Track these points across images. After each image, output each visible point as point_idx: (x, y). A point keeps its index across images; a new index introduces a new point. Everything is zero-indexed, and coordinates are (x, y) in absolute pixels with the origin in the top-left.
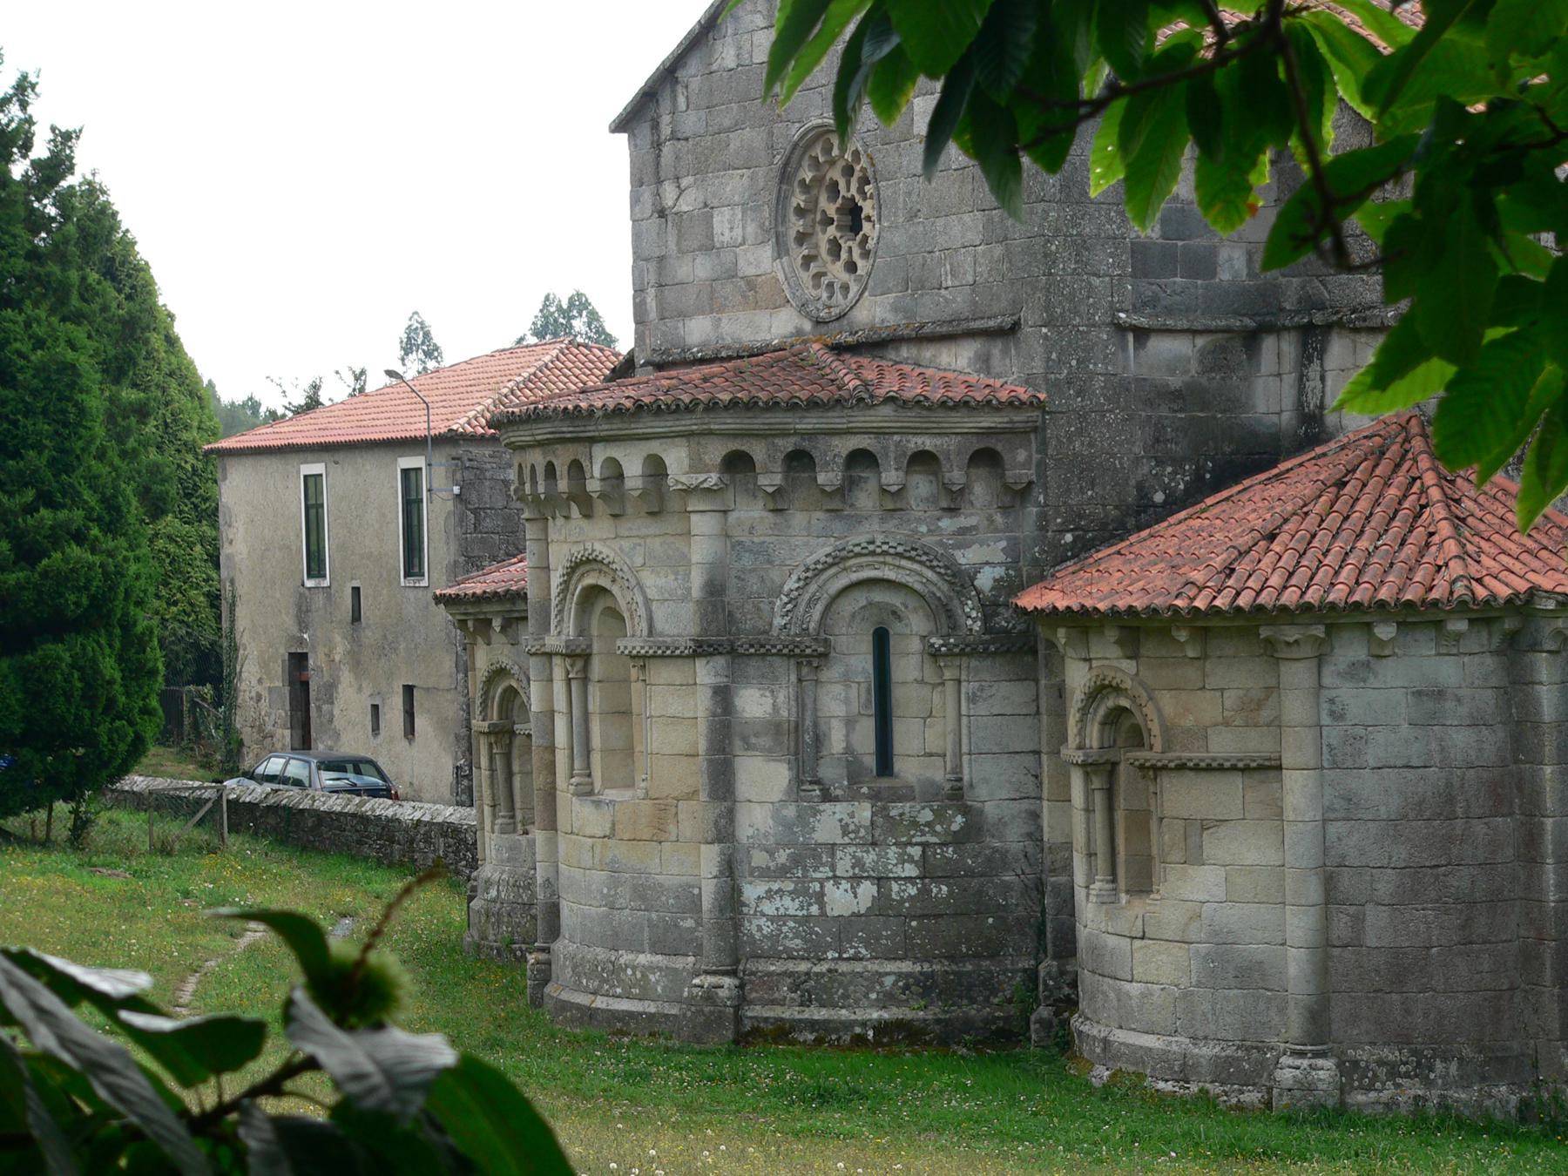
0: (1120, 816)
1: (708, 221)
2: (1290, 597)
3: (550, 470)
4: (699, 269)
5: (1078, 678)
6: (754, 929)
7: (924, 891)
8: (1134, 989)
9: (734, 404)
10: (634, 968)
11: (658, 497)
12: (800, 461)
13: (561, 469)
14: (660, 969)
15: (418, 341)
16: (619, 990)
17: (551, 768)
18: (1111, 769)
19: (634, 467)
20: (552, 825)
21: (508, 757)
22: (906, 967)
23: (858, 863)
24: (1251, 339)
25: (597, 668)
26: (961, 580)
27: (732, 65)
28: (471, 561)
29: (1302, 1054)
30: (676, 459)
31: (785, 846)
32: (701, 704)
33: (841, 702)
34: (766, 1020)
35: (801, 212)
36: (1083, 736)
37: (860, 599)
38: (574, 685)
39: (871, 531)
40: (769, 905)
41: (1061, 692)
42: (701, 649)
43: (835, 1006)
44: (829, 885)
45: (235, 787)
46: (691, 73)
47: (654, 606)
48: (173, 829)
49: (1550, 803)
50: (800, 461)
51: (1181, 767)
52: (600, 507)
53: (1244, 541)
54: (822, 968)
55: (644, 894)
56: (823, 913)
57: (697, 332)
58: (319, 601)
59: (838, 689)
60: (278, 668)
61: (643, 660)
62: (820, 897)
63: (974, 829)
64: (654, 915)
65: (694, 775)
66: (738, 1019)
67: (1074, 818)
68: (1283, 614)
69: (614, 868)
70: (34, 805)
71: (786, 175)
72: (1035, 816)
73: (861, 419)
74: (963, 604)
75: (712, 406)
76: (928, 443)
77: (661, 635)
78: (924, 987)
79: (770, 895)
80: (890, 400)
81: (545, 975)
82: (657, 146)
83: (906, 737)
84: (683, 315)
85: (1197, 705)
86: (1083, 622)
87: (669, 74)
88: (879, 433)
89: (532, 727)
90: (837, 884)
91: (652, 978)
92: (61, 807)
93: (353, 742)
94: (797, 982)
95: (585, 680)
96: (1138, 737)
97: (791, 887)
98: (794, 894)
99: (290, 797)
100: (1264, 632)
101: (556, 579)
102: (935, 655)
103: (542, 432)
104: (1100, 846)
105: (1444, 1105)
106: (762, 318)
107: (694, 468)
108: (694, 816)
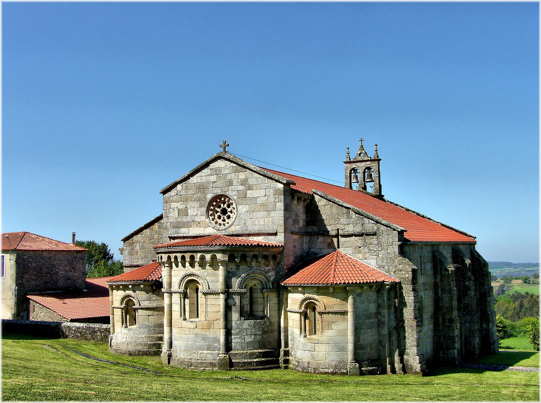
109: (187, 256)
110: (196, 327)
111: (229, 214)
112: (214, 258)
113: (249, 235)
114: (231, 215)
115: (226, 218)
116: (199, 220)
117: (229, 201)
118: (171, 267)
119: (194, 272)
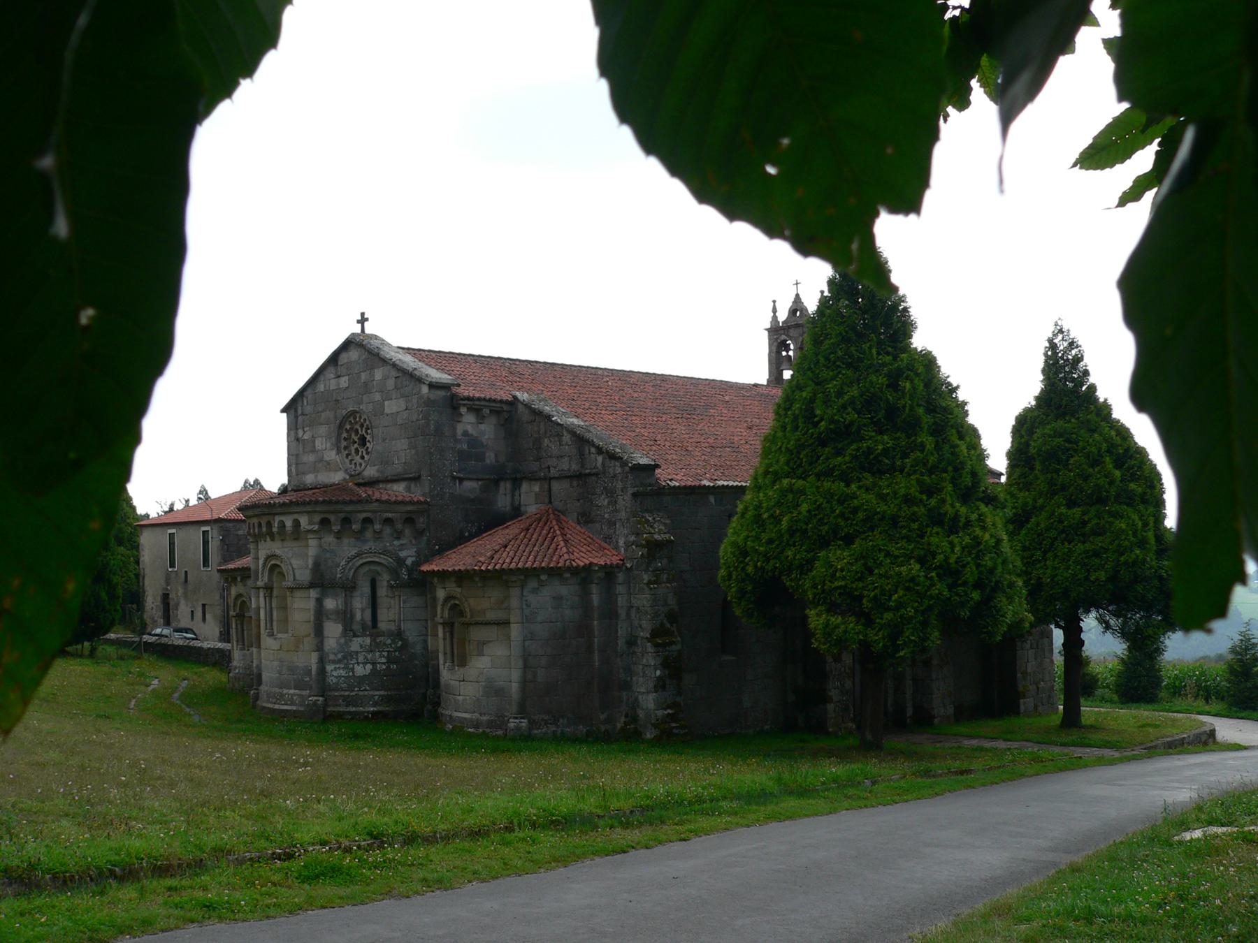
0: (455, 640)
1: (314, 442)
2: (513, 566)
3: (260, 525)
4: (311, 458)
5: (441, 594)
7: (388, 667)
8: (460, 698)
9: (324, 501)
11: (298, 533)
12: (346, 521)
13: (264, 524)
15: (203, 491)
17: (259, 626)
18: (452, 624)
19: (289, 523)
20: (259, 647)
21: (242, 625)
22: (382, 693)
24: (497, 482)
25: (275, 593)
26: (401, 562)
28: (225, 560)
30: (304, 520)
32: (312, 604)
33: (359, 604)
35: (345, 439)
36: (442, 613)
37: (366, 568)
39: (370, 545)
40: (335, 673)
41: (434, 599)
42: (312, 585)
45: (146, 638)
46: (309, 393)
48: (124, 651)
49: (596, 633)
50: (346, 521)
51: (477, 623)
52: (277, 537)
53: (497, 547)
57: (309, 479)
58: (173, 575)
59: (358, 599)
60: (159, 598)
61: (291, 589)
62: (353, 670)
63: (406, 645)
65: (309, 628)
66: (325, 712)
67: (439, 642)
68: (511, 572)
69: (281, 661)
70: (77, 643)
71: (341, 426)
72: (426, 641)
73: (367, 507)
75: (317, 502)
76: (390, 515)
80: (377, 500)
81: (257, 697)
82: (296, 417)
83: (383, 615)
84: (304, 473)
85: (483, 603)
86: (443, 575)
87: (301, 394)
89: (252, 613)
92: (87, 644)
93: (184, 622)
94: (345, 698)
95: (271, 597)
96: (462, 614)
99: (164, 640)
100: (505, 577)
101: (261, 562)
102: (391, 587)
103: (257, 511)
104: (448, 651)
105: (562, 732)
106: (332, 474)
107: (310, 523)
108: (309, 643)
112: (297, 524)
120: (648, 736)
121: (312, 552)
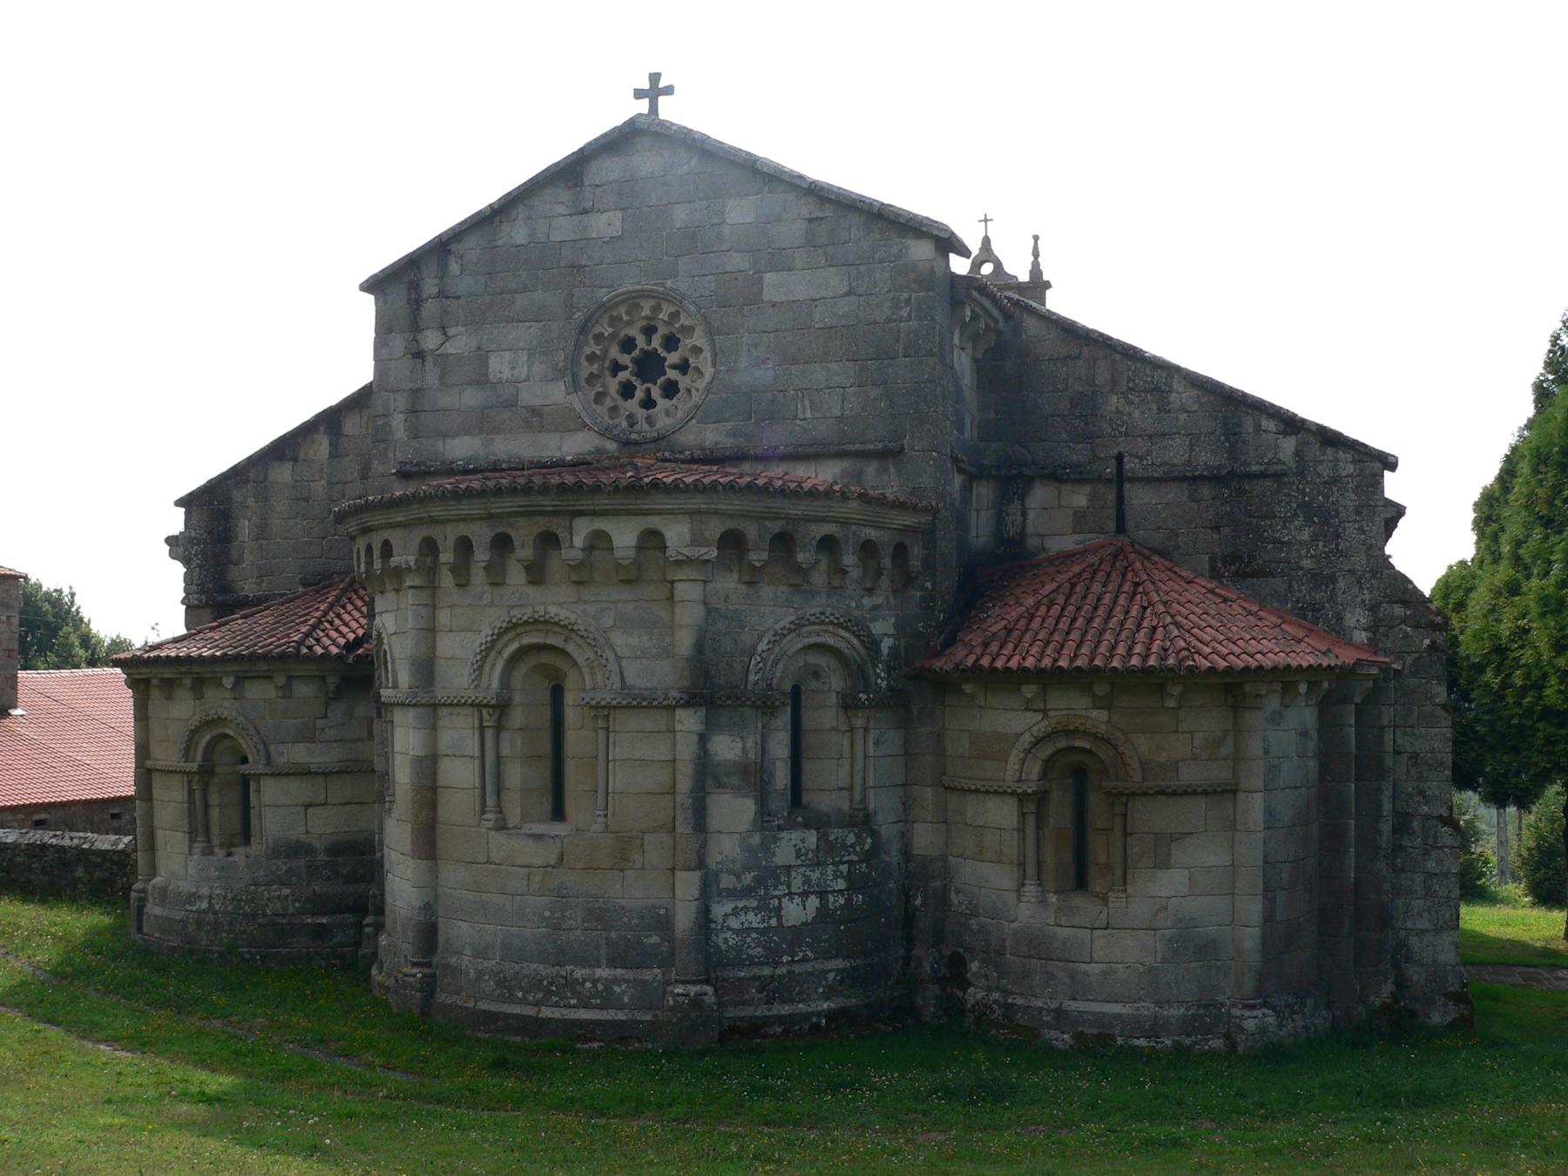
6: (720, 942)
7: (849, 900)
8: (1094, 969)
10: (595, 982)
14: (627, 981)
16: (573, 1002)
22: (840, 963)
23: (807, 881)
27: (524, 242)
29: (1253, 1007)
30: (677, 534)
31: (749, 870)
32: (686, 751)
34: (742, 1018)
37: (531, 661)
38: (489, 735)
43: (792, 1001)
44: (785, 900)
47: (624, 662)
54: (782, 970)
55: (598, 915)
56: (780, 924)
62: (778, 911)
64: (613, 935)
74: (875, 666)
77: (632, 687)
78: (850, 979)
79: (736, 912)
85: (1183, 741)
88: (844, 523)
90: (791, 899)
91: (617, 989)
94: (763, 984)
97: (755, 903)
98: (757, 910)
107: (697, 541)
109: (524, 535)
110: (561, 860)
111: (672, 374)
112: (652, 541)
113: (764, 458)
114: (683, 381)
115: (656, 393)
116: (537, 402)
117: (675, 316)
118: (432, 586)
119: (553, 610)
120: (1436, 1018)
121: (689, 614)
